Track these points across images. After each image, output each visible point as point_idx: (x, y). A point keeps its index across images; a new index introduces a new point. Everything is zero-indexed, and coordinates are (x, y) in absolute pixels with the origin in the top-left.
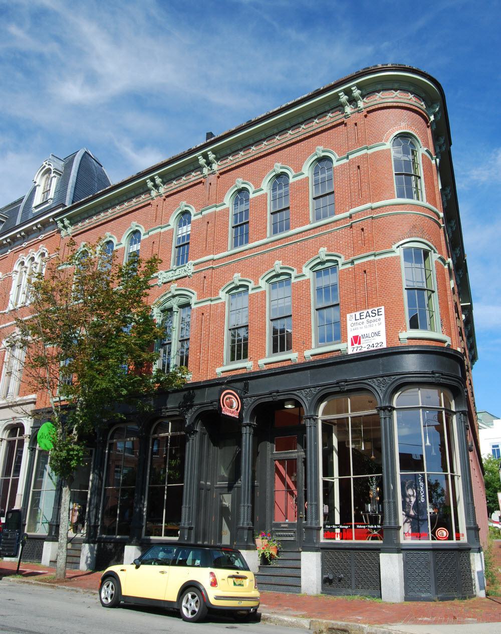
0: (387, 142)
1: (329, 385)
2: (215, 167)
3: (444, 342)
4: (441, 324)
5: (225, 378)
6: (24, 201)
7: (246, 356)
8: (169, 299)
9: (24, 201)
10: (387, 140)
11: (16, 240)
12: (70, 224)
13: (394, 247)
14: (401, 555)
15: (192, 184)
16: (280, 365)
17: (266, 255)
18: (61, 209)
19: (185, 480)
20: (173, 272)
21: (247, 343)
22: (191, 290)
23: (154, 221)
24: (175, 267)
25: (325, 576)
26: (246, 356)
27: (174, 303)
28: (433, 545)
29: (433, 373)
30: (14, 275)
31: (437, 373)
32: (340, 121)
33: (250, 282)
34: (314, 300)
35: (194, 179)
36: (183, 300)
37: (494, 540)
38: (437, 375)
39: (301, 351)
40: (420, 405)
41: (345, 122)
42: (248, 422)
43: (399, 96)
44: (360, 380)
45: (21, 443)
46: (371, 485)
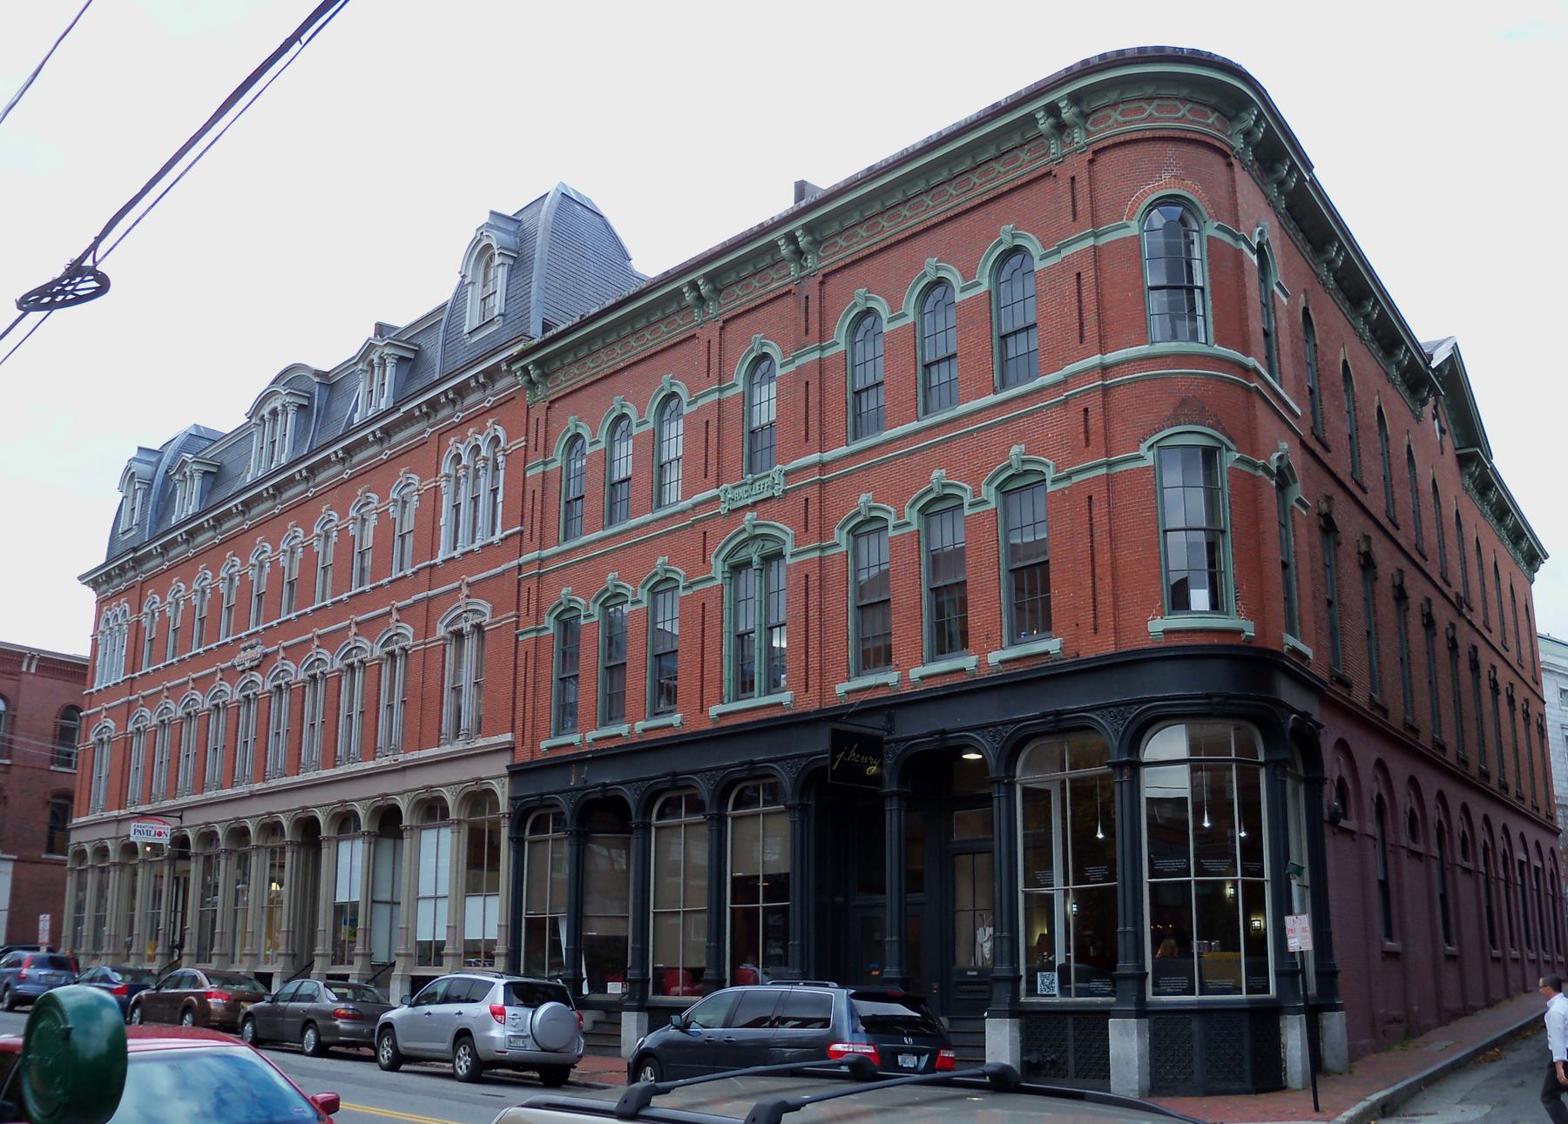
0: (1131, 220)
1: (1190, 699)
2: (811, 261)
3: (1240, 632)
4: (1236, 597)
5: (851, 705)
6: (449, 305)
7: (965, 645)
8: (743, 544)
9: (449, 305)
10: (1133, 215)
11: (438, 407)
12: (541, 376)
13: (1144, 447)
14: (1145, 1022)
15: (771, 295)
16: (948, 681)
17: (916, 458)
18: (520, 347)
19: (791, 896)
20: (746, 488)
21: (967, 616)
22: (781, 526)
23: (705, 375)
24: (109, 844)
25: (1025, 1058)
26: (965, 645)
27: (753, 553)
28: (1200, 1003)
29: (1207, 696)
30: (443, 484)
31: (1216, 696)
32: (1044, 170)
33: (890, 513)
34: (928, 577)
35: (775, 285)
36: (770, 547)
37: (193, 850)
38: (1216, 700)
39: (983, 653)
40: (1233, 757)
41: (1054, 173)
42: (895, 789)
43: (1156, 115)
44: (1082, 711)
45: (494, 834)
46: (778, 886)
